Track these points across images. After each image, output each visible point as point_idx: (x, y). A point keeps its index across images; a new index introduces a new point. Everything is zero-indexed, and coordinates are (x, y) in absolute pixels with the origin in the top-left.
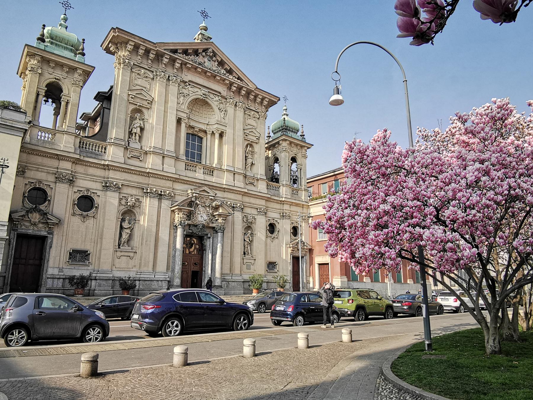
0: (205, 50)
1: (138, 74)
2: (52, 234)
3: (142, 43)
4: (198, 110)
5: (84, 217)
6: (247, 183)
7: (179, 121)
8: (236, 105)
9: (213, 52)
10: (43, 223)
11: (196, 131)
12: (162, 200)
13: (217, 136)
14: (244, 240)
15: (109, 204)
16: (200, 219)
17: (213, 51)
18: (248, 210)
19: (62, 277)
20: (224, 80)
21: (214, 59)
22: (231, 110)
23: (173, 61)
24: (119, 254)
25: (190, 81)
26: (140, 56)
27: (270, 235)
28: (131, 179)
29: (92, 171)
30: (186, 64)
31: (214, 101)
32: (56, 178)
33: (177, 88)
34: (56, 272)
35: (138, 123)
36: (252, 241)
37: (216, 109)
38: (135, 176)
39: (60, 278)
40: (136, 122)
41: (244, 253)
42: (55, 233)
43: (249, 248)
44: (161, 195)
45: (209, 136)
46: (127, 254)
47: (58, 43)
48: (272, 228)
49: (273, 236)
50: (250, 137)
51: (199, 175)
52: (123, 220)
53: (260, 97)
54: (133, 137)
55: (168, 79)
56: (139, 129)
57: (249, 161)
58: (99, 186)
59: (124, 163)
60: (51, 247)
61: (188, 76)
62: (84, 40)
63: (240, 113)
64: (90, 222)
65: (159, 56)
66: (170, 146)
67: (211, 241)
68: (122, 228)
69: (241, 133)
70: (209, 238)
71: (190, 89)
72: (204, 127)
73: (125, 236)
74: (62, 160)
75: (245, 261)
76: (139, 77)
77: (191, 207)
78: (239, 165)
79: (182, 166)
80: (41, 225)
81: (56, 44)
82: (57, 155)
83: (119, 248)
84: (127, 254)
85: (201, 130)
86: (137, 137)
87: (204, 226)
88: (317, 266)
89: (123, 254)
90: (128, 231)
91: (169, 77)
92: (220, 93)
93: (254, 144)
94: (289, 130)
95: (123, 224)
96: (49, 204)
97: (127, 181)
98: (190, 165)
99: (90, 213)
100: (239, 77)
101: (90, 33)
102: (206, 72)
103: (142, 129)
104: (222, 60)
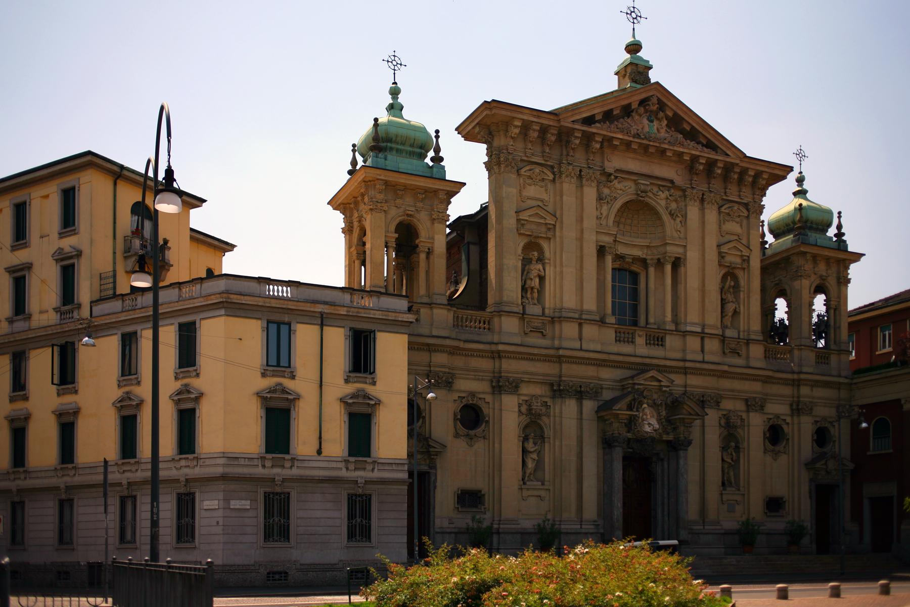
0: (643, 102)
1: (728, 214)
2: (435, 468)
3: (535, 120)
4: (629, 221)
5: (471, 439)
6: (527, 330)
7: (601, 251)
8: (702, 198)
9: (660, 101)
10: (422, 453)
11: (628, 263)
12: (503, 396)
13: (668, 268)
14: (723, 460)
15: (509, 416)
16: (648, 429)
17: (659, 99)
18: (727, 405)
19: (453, 530)
20: (681, 154)
21: (661, 114)
22: (693, 212)
23: (588, 138)
24: (525, 493)
25: (617, 171)
26: (512, 138)
27: (771, 447)
28: (533, 370)
29: (475, 363)
30: (611, 139)
31: (660, 200)
32: (555, 391)
33: (595, 189)
34: (446, 524)
35: (536, 268)
36: (737, 461)
37: (666, 217)
38: (538, 364)
39: (450, 533)
40: (532, 267)
41: (723, 484)
42: (438, 466)
43: (732, 473)
44: (581, 392)
45: (652, 270)
46: (536, 493)
47: (400, 147)
48: (775, 435)
49: (777, 448)
50: (729, 259)
51: (640, 348)
52: (525, 439)
53: (720, 165)
54: (529, 295)
55: (580, 177)
56: (537, 280)
57: (730, 307)
58: (740, 406)
59: (581, 349)
60: (435, 487)
61: (615, 162)
62: (437, 132)
63: (712, 215)
64: (480, 446)
65: (564, 136)
66: (590, 304)
67: (666, 466)
68: (525, 451)
69: (712, 255)
70: (662, 460)
71: (618, 186)
72: (637, 253)
73: (530, 465)
74: (435, 351)
75: (725, 498)
76: (529, 181)
77: (631, 410)
78: (713, 318)
79: (610, 334)
80: (419, 456)
81: (398, 150)
82: (428, 345)
83: (524, 483)
84: (536, 493)
85: (636, 259)
86: (536, 295)
87: (653, 439)
88: (866, 503)
89: (530, 493)
90: (535, 456)
91: (580, 171)
92: (672, 182)
93: (545, 245)
94: (811, 228)
95: (526, 445)
96: (424, 422)
97: (527, 373)
98: (622, 331)
99: (479, 431)
100: (709, 140)
101: (438, 111)
102: (646, 148)
103: (542, 279)
104: (675, 114)
